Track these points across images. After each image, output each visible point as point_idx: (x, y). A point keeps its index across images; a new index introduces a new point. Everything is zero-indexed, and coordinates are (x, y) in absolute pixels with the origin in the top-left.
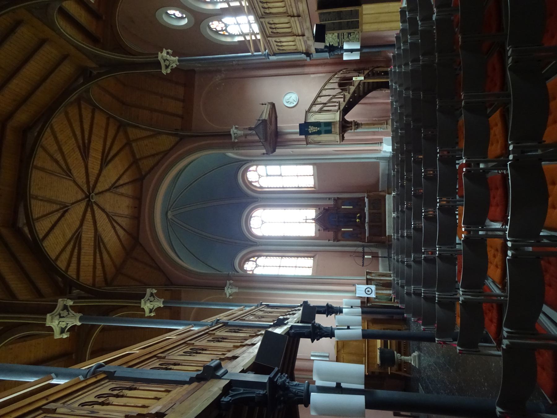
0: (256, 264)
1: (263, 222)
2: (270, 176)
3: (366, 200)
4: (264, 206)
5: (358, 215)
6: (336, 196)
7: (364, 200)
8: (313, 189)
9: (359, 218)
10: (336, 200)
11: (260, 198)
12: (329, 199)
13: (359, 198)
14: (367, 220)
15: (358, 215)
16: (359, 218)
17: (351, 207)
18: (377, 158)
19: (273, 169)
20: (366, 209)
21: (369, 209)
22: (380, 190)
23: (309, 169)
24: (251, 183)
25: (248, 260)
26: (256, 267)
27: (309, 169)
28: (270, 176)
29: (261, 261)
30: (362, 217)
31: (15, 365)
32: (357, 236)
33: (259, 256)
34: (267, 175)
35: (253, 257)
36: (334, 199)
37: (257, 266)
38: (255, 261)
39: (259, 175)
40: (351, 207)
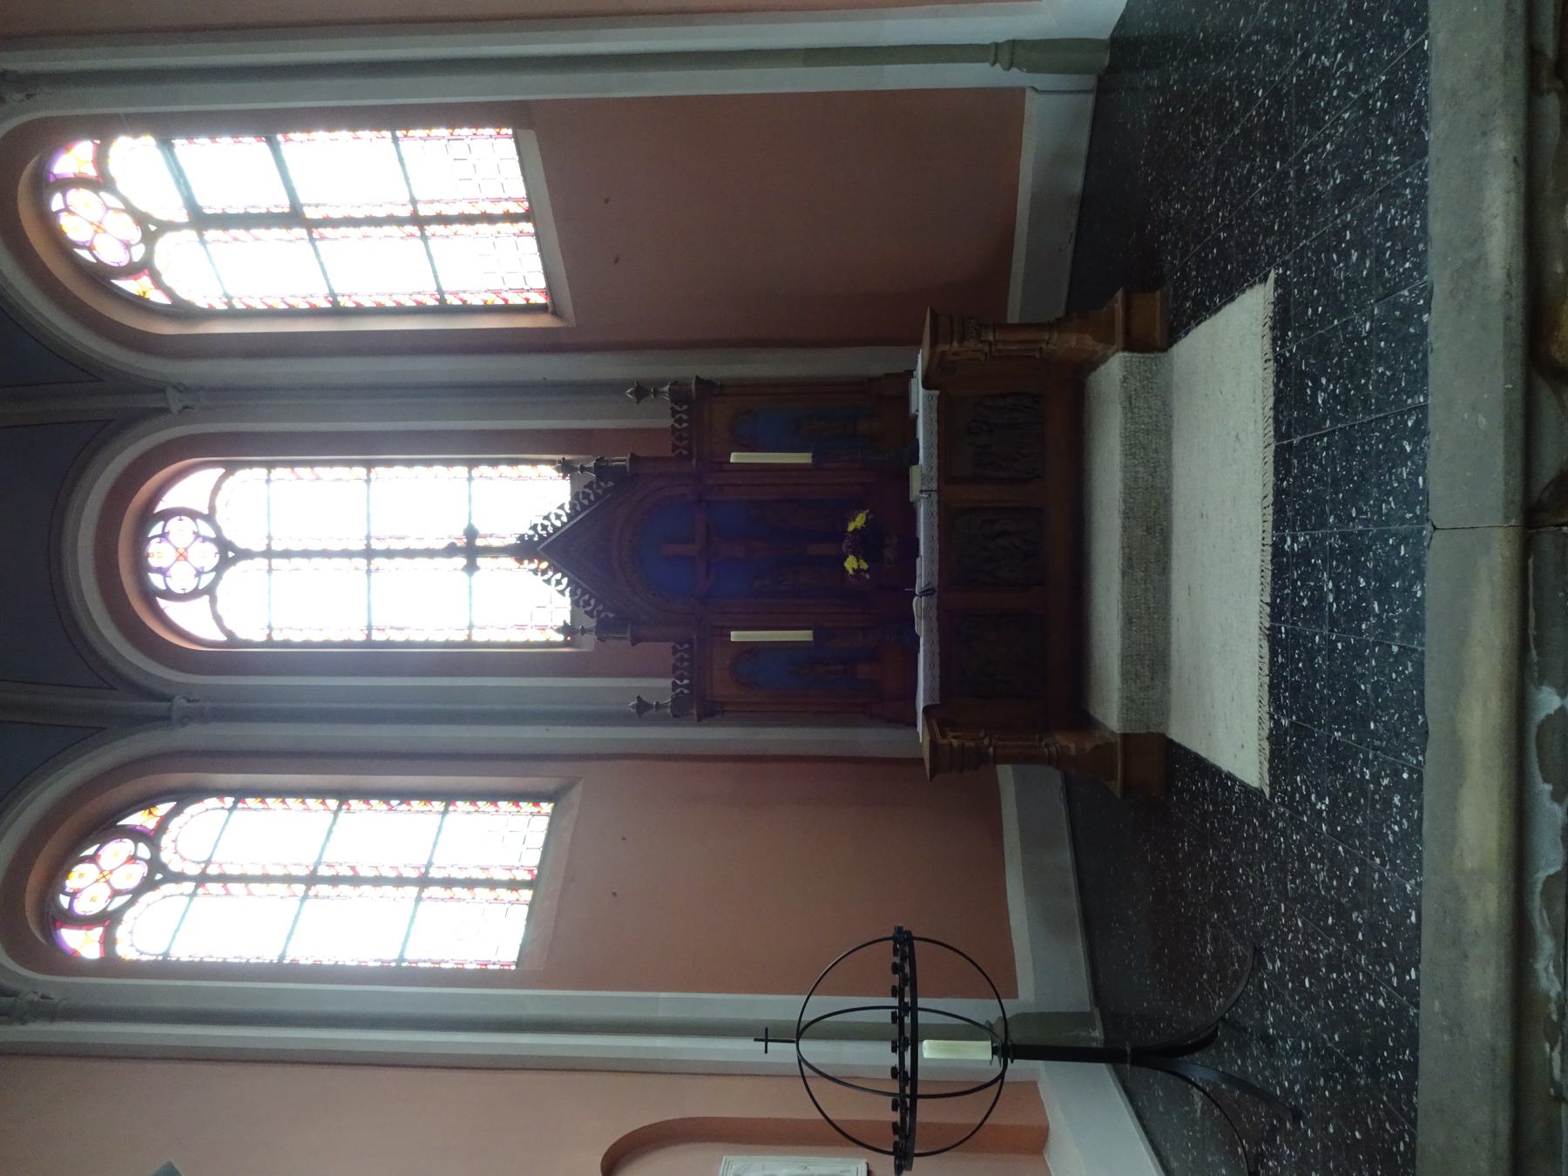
0: (155, 864)
1: (228, 554)
2: (225, 221)
3: (920, 399)
4: (233, 449)
5: (859, 521)
6: (690, 368)
7: (904, 398)
8: (545, 321)
9: (865, 544)
10: (694, 400)
11: (182, 389)
12: (641, 391)
13: (863, 387)
14: (924, 571)
15: (859, 521)
16: (865, 544)
17: (804, 458)
18: (1011, 52)
19: (228, 166)
20: (922, 477)
21: (947, 475)
22: (1013, 317)
23: (484, 165)
24: (99, 276)
25: (105, 827)
26: (148, 884)
27: (484, 165)
28: (225, 221)
29: (201, 830)
30: (891, 540)
31: (1436, 227)
32: (850, 678)
33: (186, 796)
34: (201, 220)
35: (146, 802)
36: (679, 394)
37: (157, 875)
38: (150, 838)
39: (141, 219)
40: (804, 458)
